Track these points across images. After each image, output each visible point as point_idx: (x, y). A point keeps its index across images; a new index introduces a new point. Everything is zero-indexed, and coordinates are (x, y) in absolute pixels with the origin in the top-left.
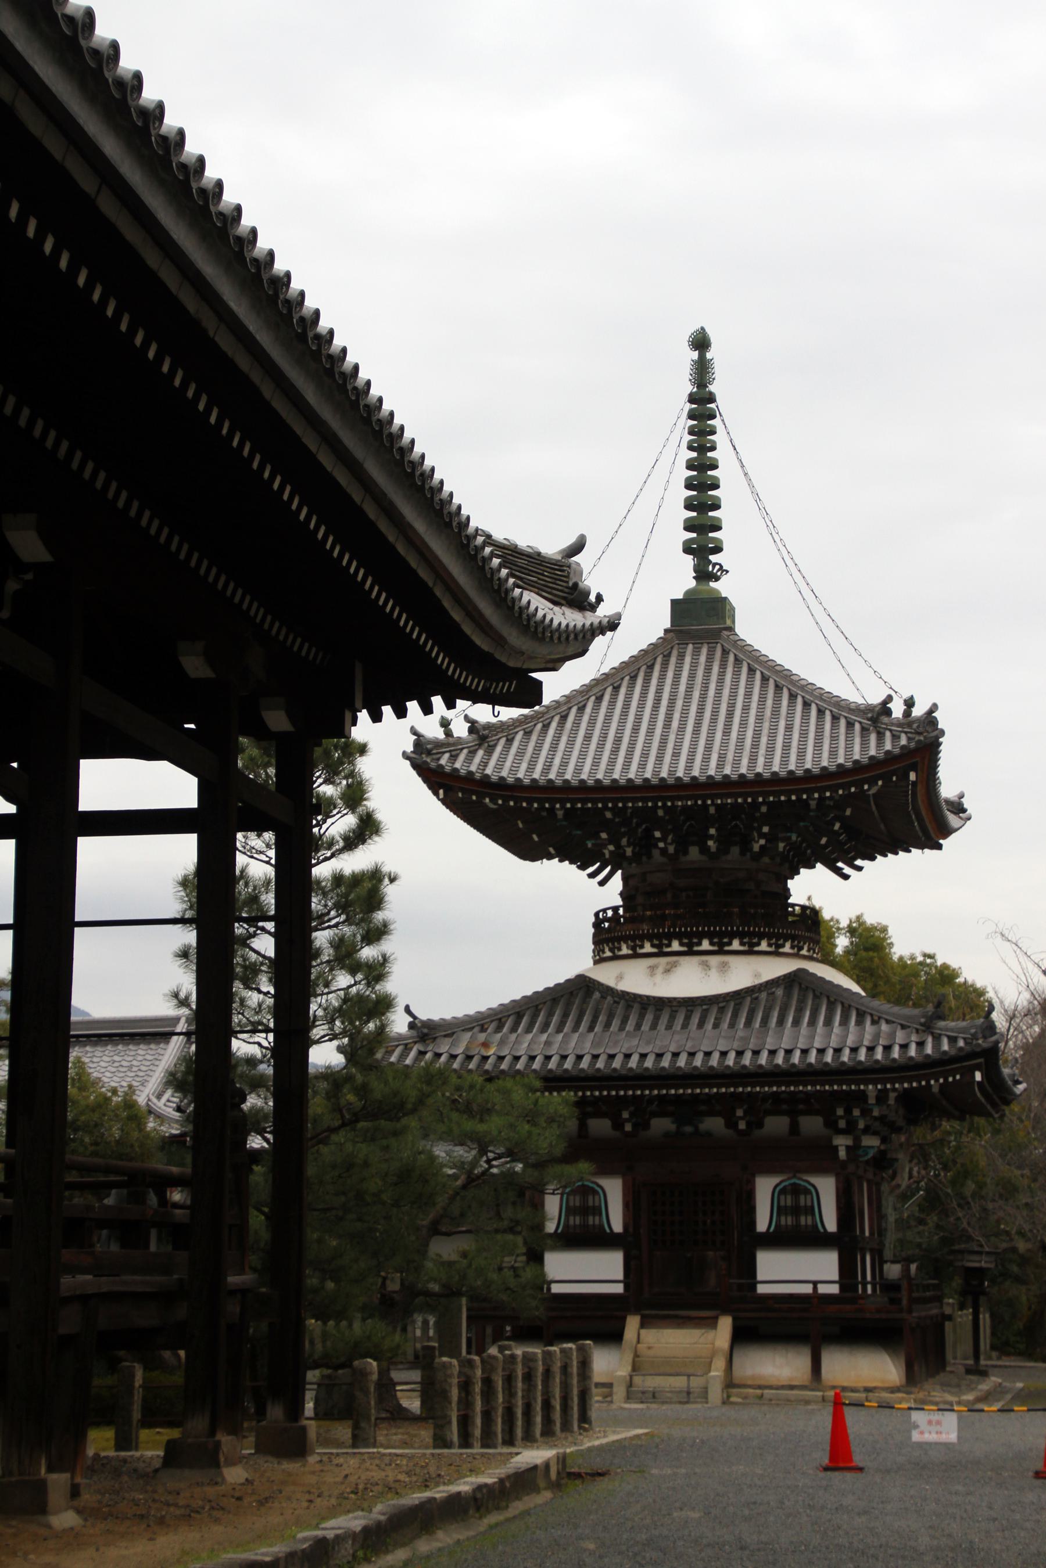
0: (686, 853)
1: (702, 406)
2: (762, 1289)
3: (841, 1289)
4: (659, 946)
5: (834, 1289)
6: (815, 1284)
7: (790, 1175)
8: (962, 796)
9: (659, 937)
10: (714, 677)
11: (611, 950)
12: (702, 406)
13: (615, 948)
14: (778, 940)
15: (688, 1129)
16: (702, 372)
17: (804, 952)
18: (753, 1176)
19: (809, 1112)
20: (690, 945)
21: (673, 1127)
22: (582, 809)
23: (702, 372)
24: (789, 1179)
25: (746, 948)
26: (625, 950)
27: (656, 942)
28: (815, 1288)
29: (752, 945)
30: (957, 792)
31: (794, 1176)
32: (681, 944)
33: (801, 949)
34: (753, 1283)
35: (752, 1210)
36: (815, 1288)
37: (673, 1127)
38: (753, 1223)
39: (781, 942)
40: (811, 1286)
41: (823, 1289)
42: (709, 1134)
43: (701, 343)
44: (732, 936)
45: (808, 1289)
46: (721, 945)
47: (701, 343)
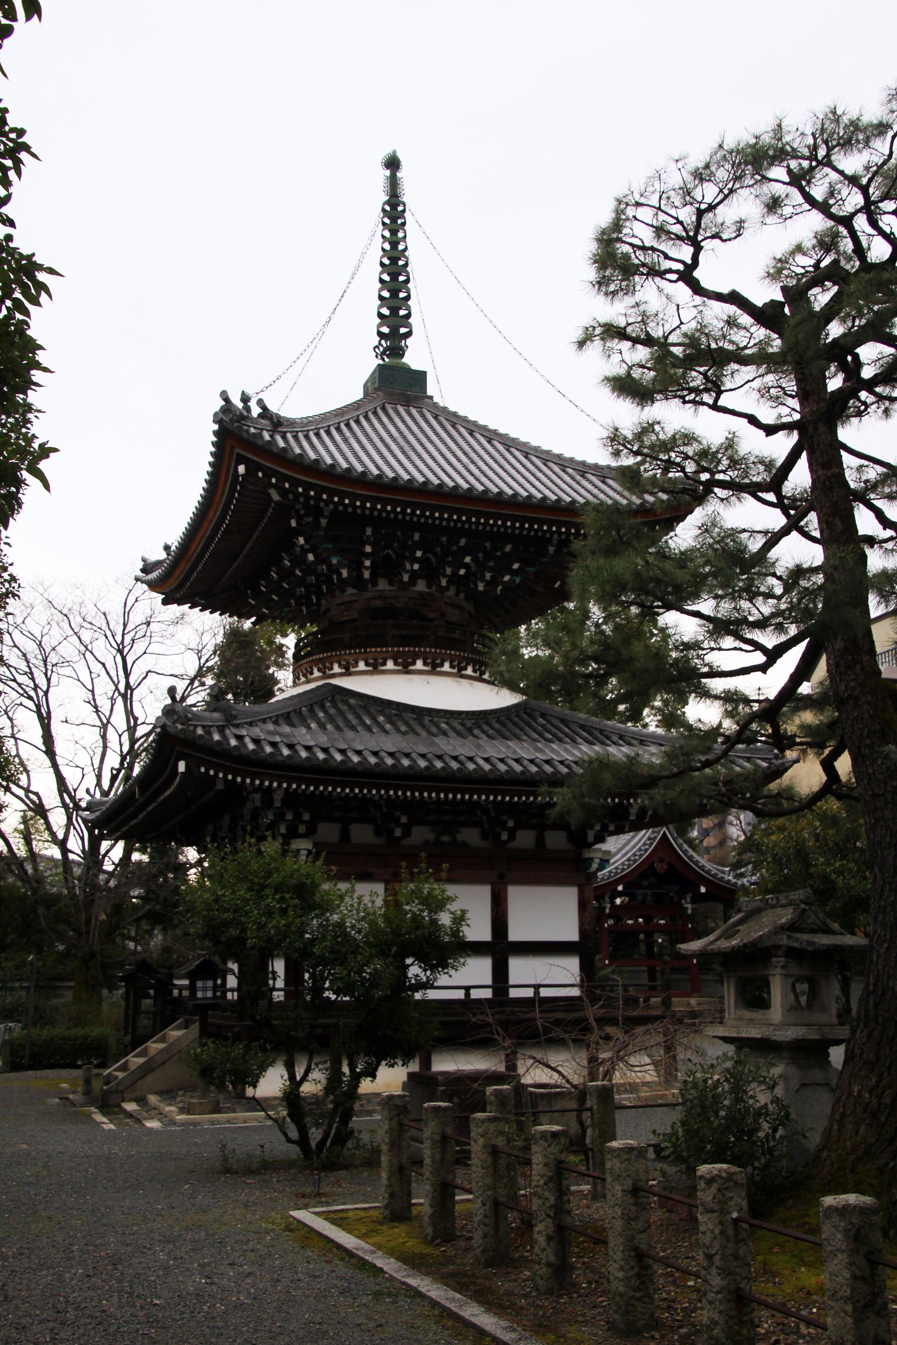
0: (415, 584)
1: (394, 213)
5: (487, 994)
8: (144, 560)
9: (322, 661)
10: (352, 441)
12: (394, 213)
15: (445, 839)
16: (393, 185)
17: (486, 677)
19: (361, 820)
20: (347, 668)
21: (431, 836)
22: (313, 550)
23: (393, 185)
25: (477, 675)
28: (467, 994)
29: (460, 670)
33: (482, 673)
36: (467, 994)
37: (431, 836)
40: (463, 992)
41: (475, 994)
42: (465, 844)
43: (393, 164)
45: (460, 995)
47: (393, 164)
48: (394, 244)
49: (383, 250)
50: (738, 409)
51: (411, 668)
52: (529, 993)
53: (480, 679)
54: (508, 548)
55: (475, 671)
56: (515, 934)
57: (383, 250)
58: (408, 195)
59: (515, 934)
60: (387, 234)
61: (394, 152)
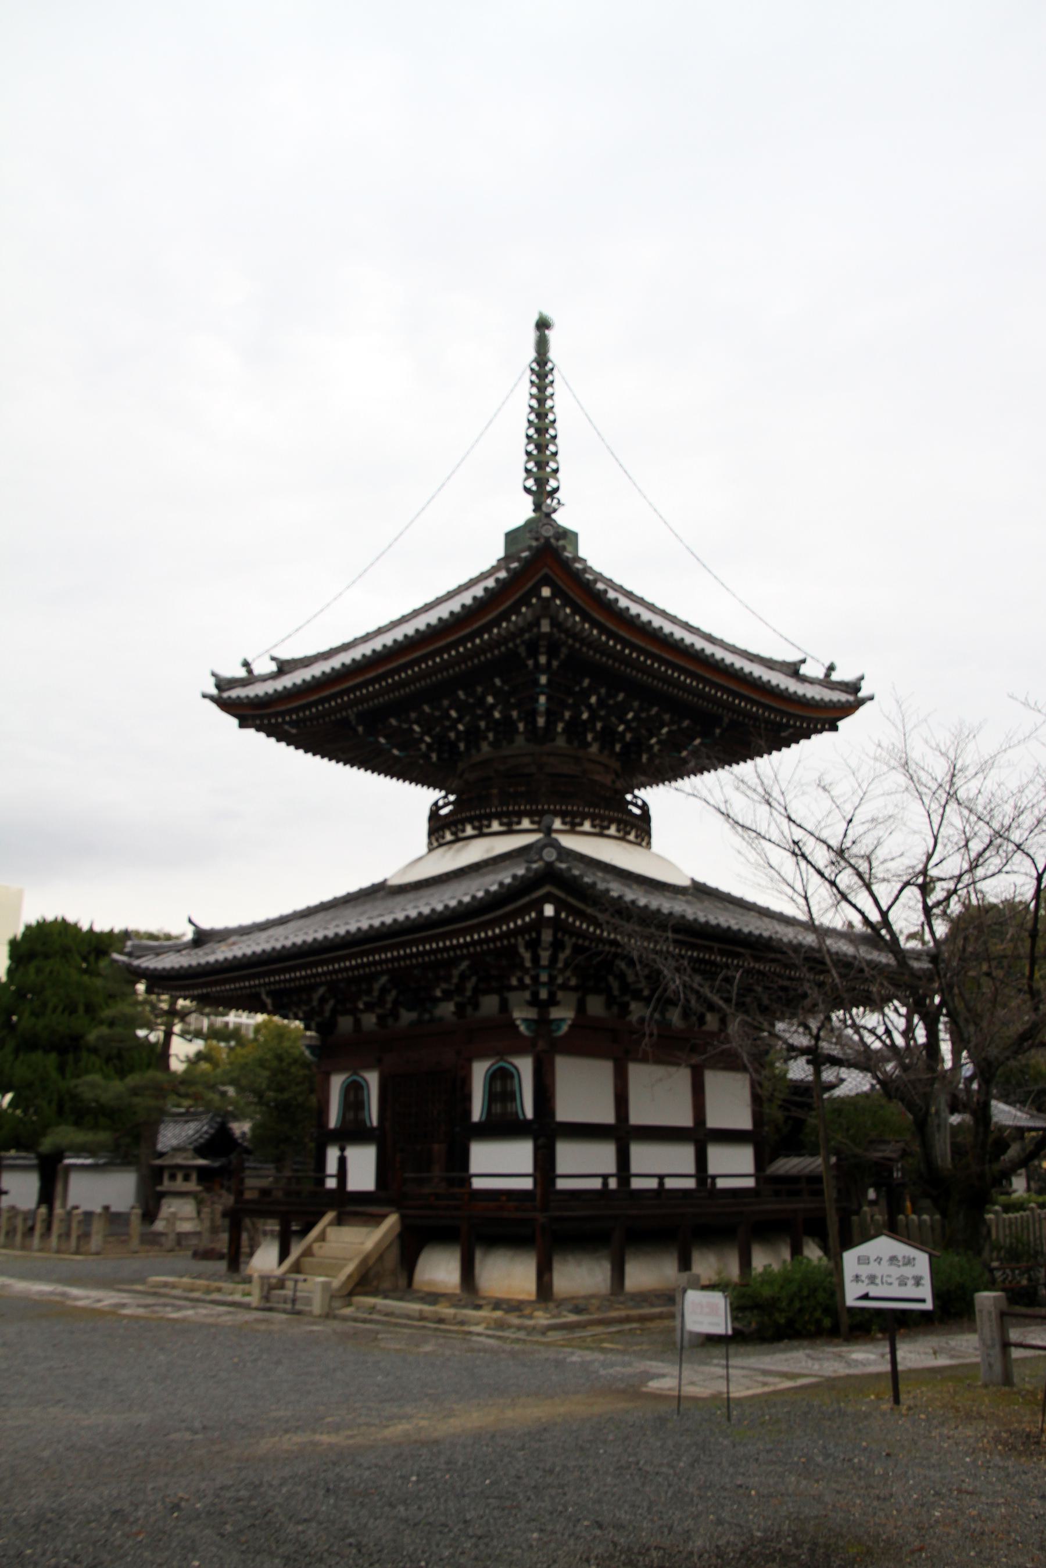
2: (478, 1184)
3: (757, 1182)
4: (509, 824)
6: (661, 1178)
7: (498, 1058)
11: (453, 834)
12: (542, 370)
13: (458, 830)
14: (574, 818)
15: (427, 1016)
16: (542, 346)
18: (469, 1061)
20: (479, 828)
23: (542, 346)
24: (497, 1062)
25: (597, 830)
26: (469, 831)
27: (477, 824)
28: (661, 1184)
29: (573, 825)
30: (858, 675)
31: (502, 1059)
32: (501, 824)
34: (467, 1179)
35: (468, 1098)
36: (661, 1184)
38: (468, 1112)
39: (578, 820)
41: (670, 1184)
44: (490, 817)
46: (509, 824)
47: (543, 325)
48: (542, 401)
49: (531, 407)
50: (530, 354)
51: (579, 829)
52: (652, 1184)
53: (623, 839)
54: (586, 682)
55: (618, 830)
56: (637, 1117)
57: (531, 407)
58: (554, 354)
59: (637, 1117)
60: (534, 391)
61: (541, 314)
